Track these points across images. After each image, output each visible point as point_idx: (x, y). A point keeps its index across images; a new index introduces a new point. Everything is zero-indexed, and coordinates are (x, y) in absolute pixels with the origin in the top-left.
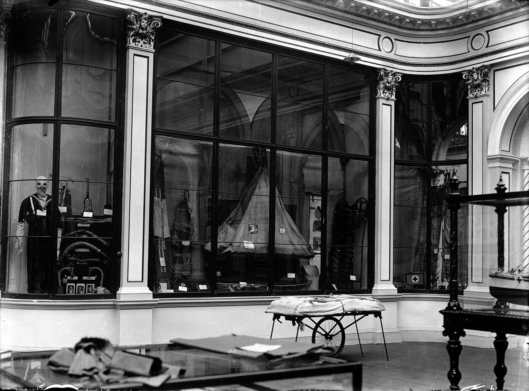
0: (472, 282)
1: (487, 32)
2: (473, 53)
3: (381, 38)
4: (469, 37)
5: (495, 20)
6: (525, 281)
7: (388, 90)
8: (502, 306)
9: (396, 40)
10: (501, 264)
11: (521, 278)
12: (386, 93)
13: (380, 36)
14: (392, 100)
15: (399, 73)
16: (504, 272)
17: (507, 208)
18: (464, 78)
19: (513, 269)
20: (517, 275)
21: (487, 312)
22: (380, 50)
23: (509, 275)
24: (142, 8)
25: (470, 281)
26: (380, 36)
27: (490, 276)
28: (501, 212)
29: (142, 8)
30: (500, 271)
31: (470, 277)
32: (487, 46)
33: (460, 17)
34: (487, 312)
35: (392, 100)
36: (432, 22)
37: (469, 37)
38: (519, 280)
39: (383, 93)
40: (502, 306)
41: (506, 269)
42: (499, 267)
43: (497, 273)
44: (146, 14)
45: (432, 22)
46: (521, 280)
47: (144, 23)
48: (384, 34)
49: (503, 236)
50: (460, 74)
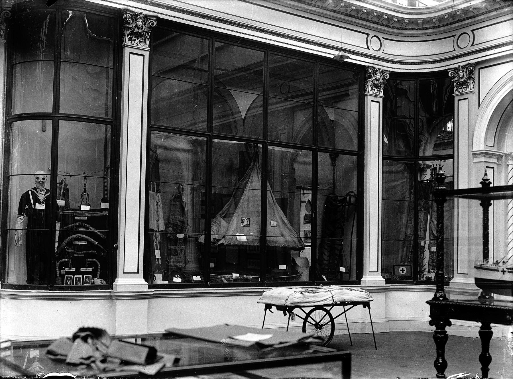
0: (458, 273)
1: (472, 31)
2: (458, 52)
3: (370, 37)
4: (455, 36)
5: (480, 20)
6: (509, 272)
7: (377, 87)
8: (487, 297)
9: (384, 38)
10: (486, 255)
11: (505, 270)
12: (374, 90)
13: (368, 34)
14: (380, 97)
15: (387, 71)
16: (489, 263)
17: (492, 202)
18: (450, 75)
19: (497, 261)
20: (501, 266)
21: (473, 302)
22: (368, 48)
23: (494, 267)
24: (138, 8)
25: (455, 272)
26: (368, 34)
27: (475, 267)
28: (486, 206)
29: (138, 8)
30: (485, 263)
31: (455, 269)
32: (472, 45)
33: (446, 17)
34: (473, 302)
35: (380, 97)
36: (419, 22)
37: (455, 36)
38: (503, 271)
39: (372, 90)
40: (487, 297)
41: (491, 260)
42: (484, 259)
43: (481, 265)
44: (141, 13)
45: (419, 22)
46: (505, 271)
47: (140, 23)
48: (372, 33)
49: (488, 229)
50: (446, 72)
